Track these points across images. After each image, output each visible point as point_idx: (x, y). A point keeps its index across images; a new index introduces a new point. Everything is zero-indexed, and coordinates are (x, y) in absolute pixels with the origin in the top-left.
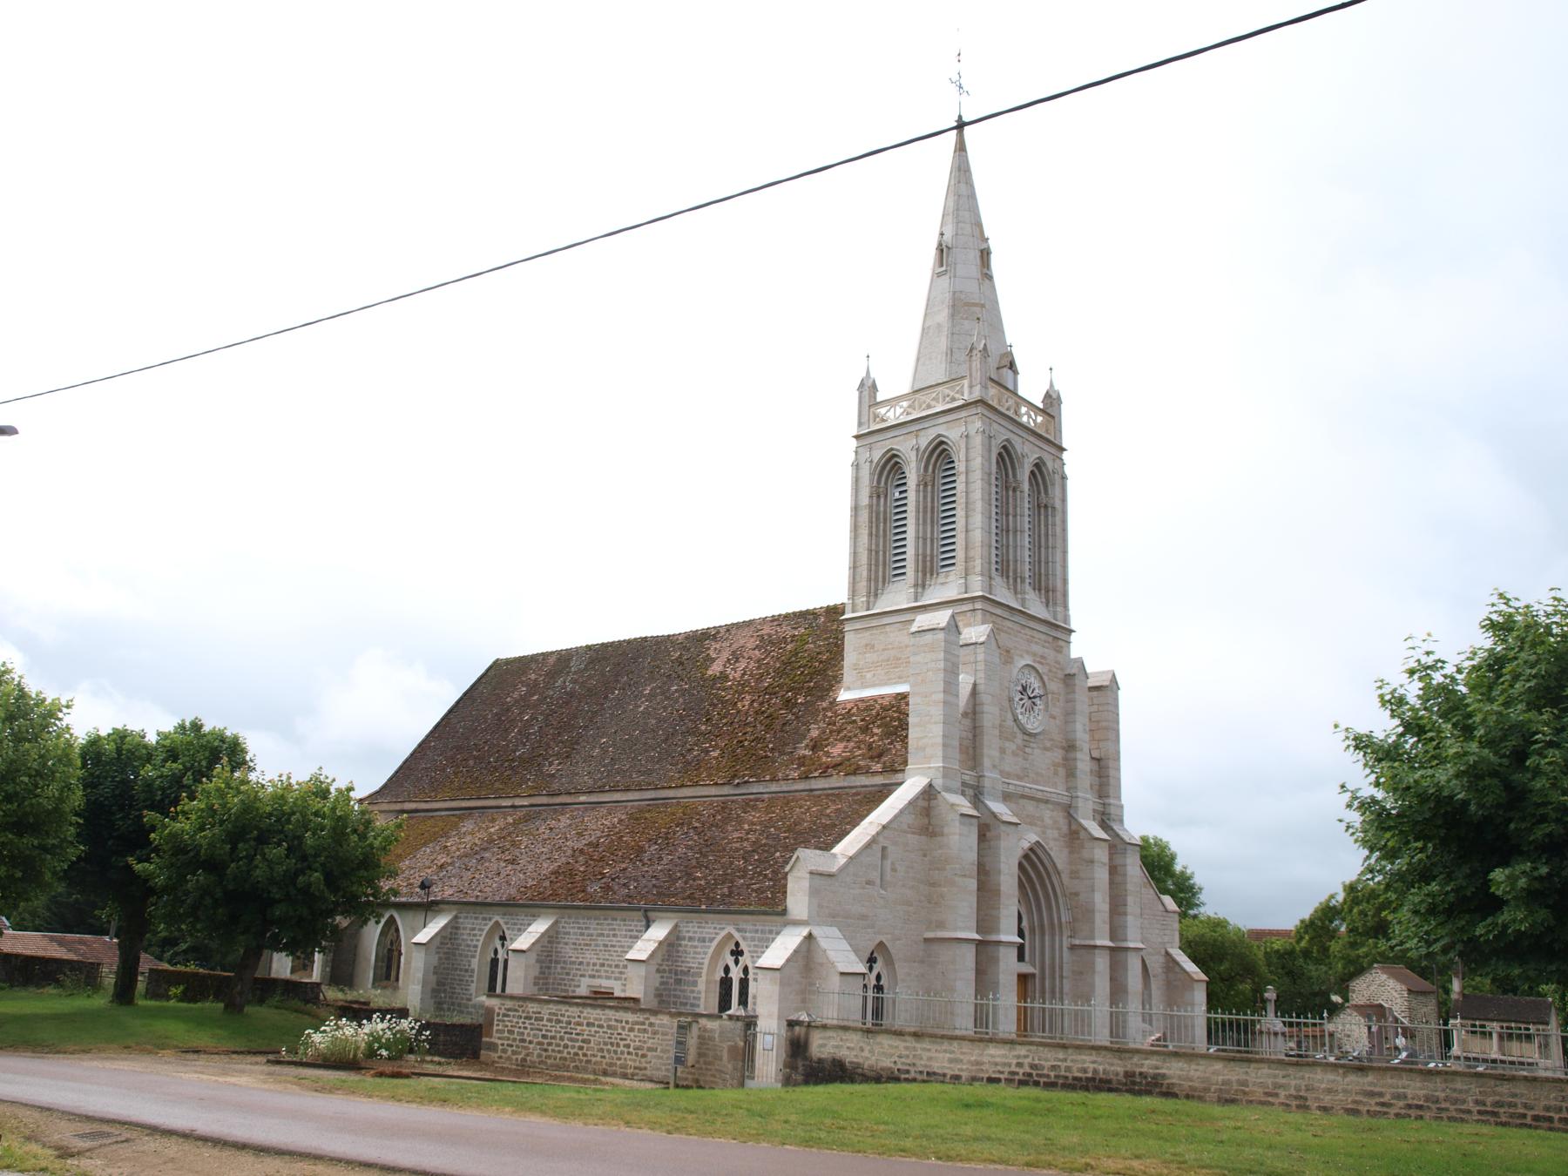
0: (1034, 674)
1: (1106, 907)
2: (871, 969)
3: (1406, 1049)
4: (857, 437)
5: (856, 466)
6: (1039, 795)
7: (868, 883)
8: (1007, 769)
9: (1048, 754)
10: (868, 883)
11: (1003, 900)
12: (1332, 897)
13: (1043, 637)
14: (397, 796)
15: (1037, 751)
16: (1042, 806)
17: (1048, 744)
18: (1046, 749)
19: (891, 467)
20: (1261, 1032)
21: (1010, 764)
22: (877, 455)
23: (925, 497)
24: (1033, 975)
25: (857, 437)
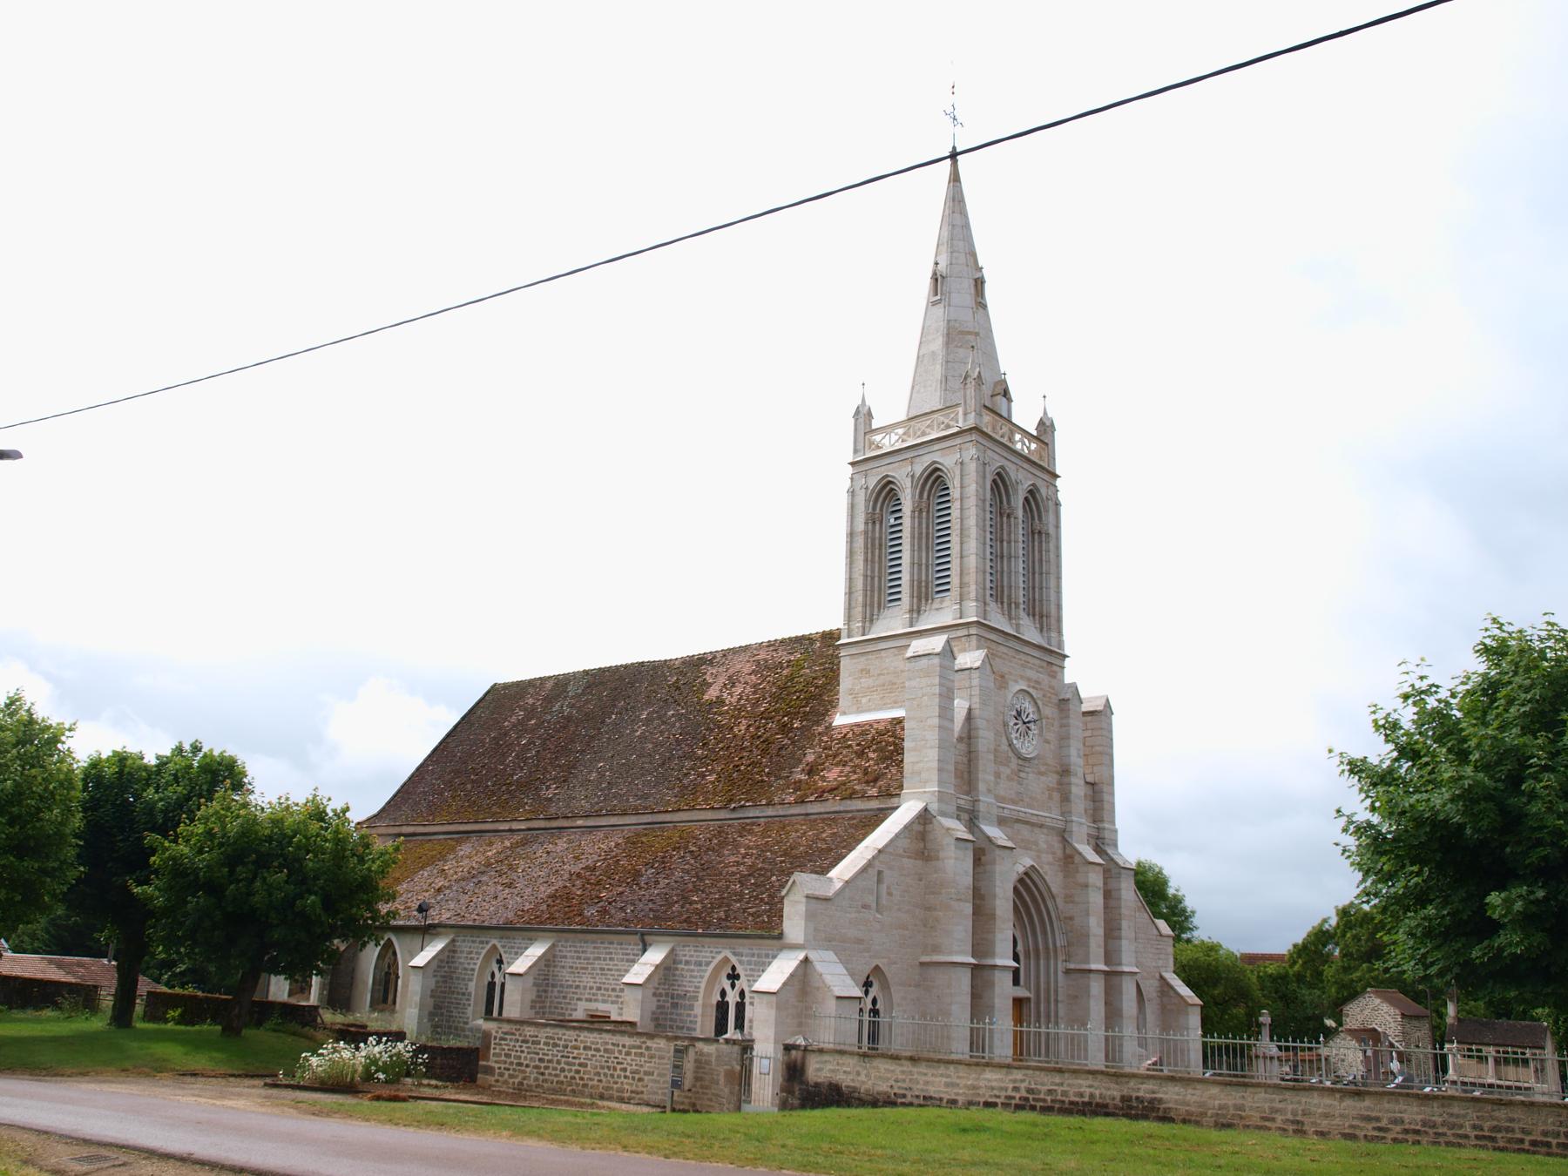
0: (1028, 699)
1: (1101, 932)
2: (867, 993)
5: (852, 493)
7: (865, 907)
8: (1002, 793)
9: (1043, 778)
10: (865, 907)
15: (1031, 776)
16: (1037, 830)
17: (1043, 769)
19: (886, 493)
22: (873, 481)
23: (920, 524)
24: (1028, 999)
25: (853, 464)
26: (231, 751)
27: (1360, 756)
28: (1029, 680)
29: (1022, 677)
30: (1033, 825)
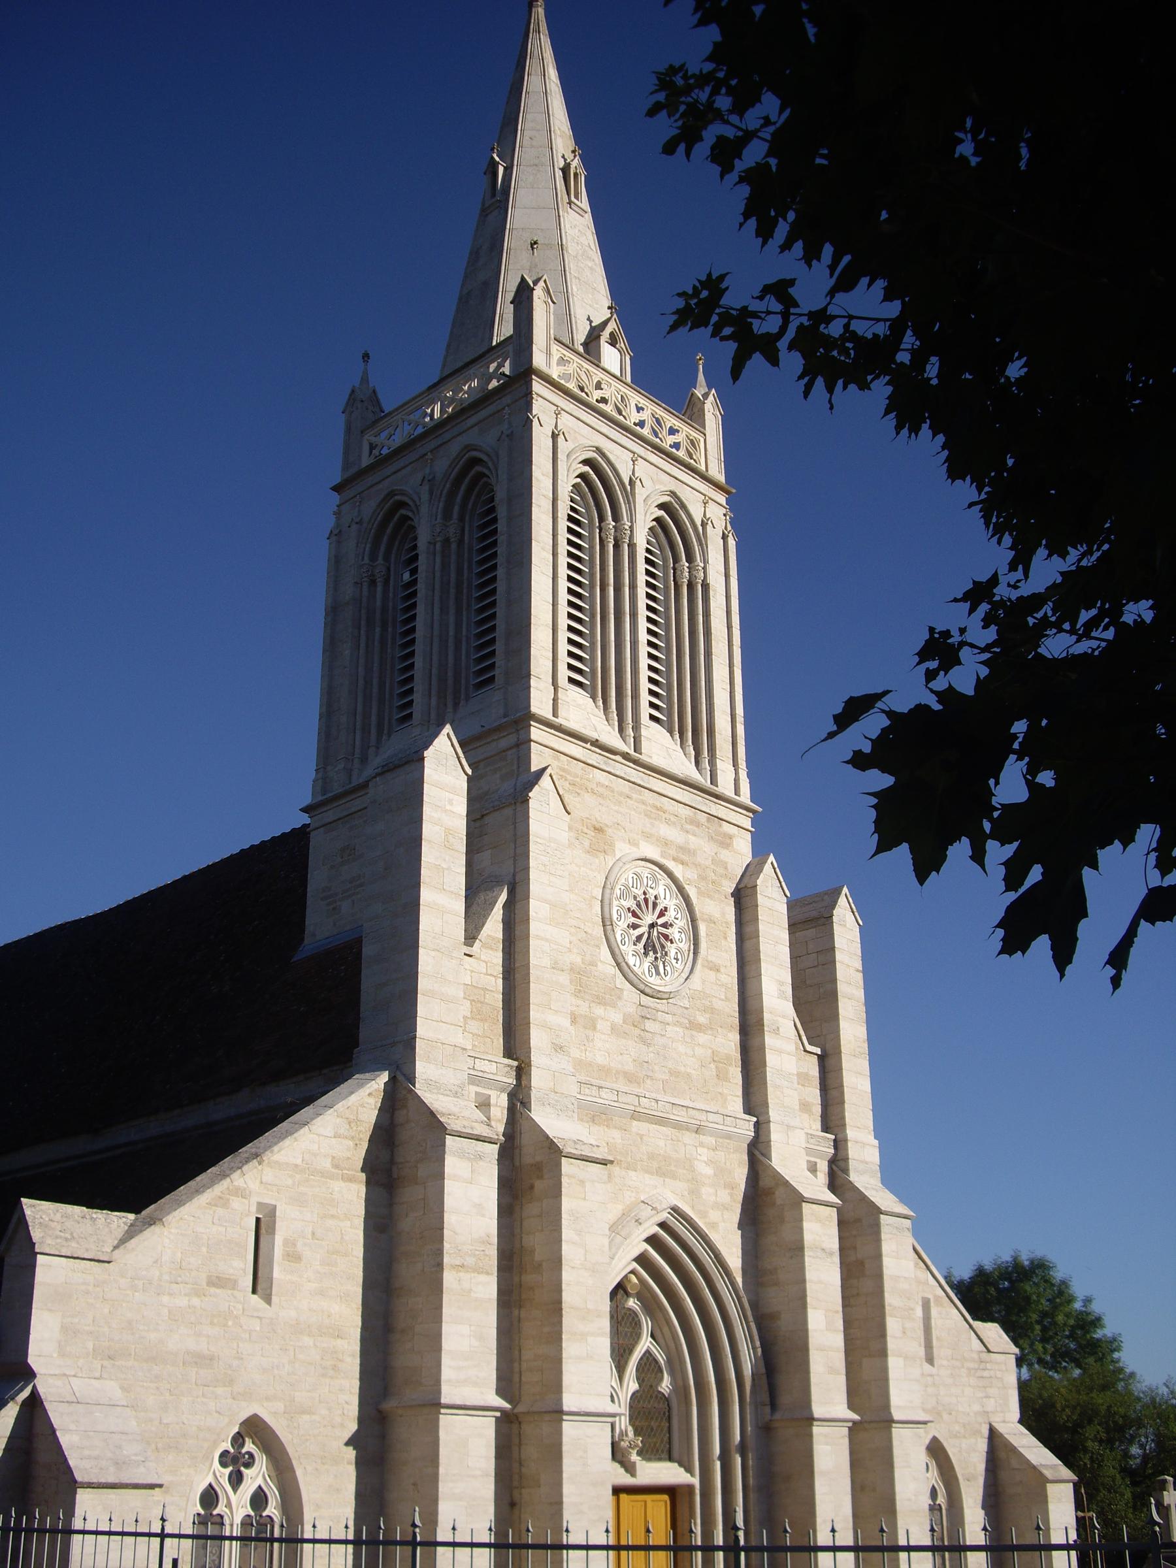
0: (664, 880)
1: (839, 1340)
2: (236, 1480)
3: (715, 92)
4: (337, 489)
5: (337, 535)
6: (679, 1115)
7: (217, 1282)
8: (600, 1059)
9: (702, 1038)
10: (217, 1282)
11: (570, 1322)
12: (997, 783)
13: (685, 812)
14: (743, 1449)
15: (674, 1031)
16: (689, 1138)
17: (702, 1019)
18: (694, 1026)
19: (394, 527)
20: (390, 1542)
21: (603, 1049)
22: (369, 507)
23: (445, 566)
24: (690, 1488)
25: (337, 489)
26: (923, 1449)
27: (667, 66)
28: (665, 843)
29: (647, 836)
30: (678, 1126)
